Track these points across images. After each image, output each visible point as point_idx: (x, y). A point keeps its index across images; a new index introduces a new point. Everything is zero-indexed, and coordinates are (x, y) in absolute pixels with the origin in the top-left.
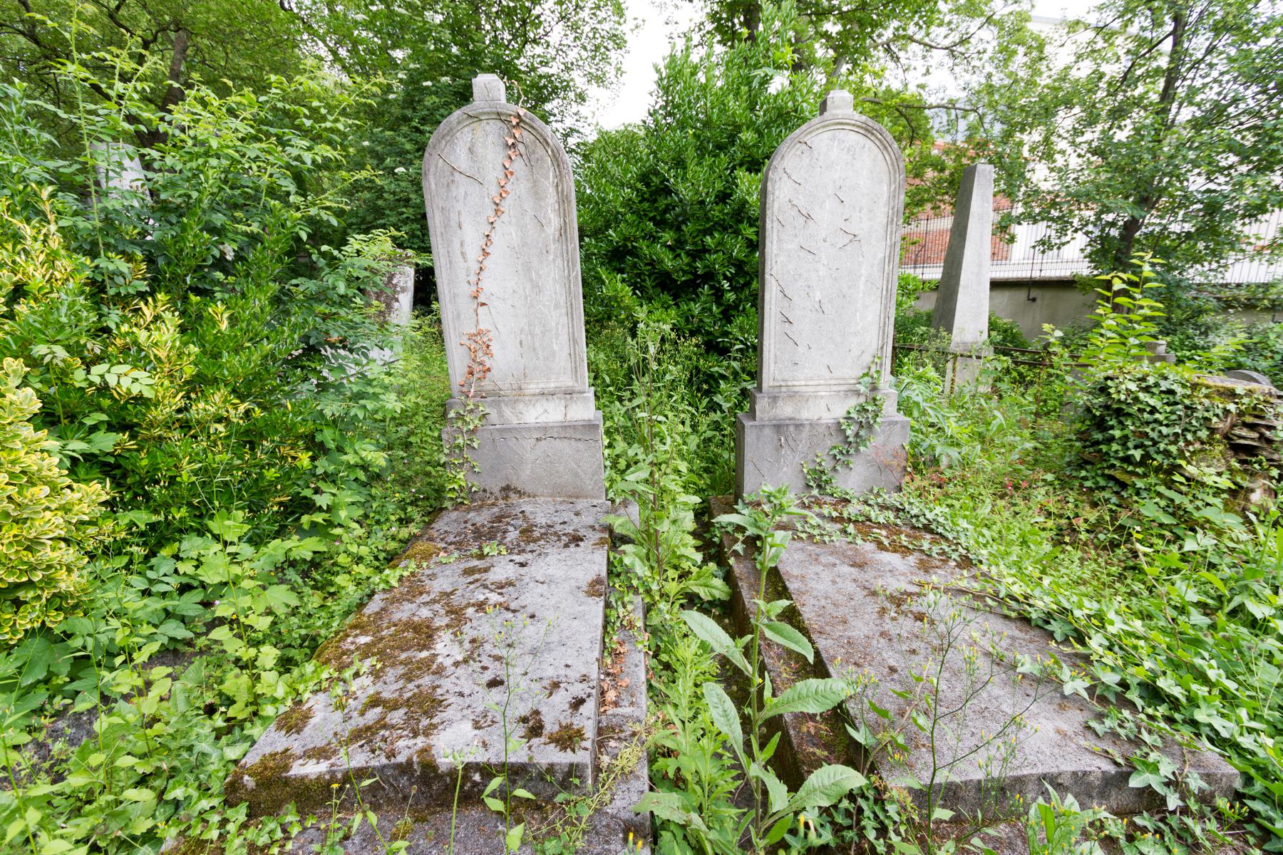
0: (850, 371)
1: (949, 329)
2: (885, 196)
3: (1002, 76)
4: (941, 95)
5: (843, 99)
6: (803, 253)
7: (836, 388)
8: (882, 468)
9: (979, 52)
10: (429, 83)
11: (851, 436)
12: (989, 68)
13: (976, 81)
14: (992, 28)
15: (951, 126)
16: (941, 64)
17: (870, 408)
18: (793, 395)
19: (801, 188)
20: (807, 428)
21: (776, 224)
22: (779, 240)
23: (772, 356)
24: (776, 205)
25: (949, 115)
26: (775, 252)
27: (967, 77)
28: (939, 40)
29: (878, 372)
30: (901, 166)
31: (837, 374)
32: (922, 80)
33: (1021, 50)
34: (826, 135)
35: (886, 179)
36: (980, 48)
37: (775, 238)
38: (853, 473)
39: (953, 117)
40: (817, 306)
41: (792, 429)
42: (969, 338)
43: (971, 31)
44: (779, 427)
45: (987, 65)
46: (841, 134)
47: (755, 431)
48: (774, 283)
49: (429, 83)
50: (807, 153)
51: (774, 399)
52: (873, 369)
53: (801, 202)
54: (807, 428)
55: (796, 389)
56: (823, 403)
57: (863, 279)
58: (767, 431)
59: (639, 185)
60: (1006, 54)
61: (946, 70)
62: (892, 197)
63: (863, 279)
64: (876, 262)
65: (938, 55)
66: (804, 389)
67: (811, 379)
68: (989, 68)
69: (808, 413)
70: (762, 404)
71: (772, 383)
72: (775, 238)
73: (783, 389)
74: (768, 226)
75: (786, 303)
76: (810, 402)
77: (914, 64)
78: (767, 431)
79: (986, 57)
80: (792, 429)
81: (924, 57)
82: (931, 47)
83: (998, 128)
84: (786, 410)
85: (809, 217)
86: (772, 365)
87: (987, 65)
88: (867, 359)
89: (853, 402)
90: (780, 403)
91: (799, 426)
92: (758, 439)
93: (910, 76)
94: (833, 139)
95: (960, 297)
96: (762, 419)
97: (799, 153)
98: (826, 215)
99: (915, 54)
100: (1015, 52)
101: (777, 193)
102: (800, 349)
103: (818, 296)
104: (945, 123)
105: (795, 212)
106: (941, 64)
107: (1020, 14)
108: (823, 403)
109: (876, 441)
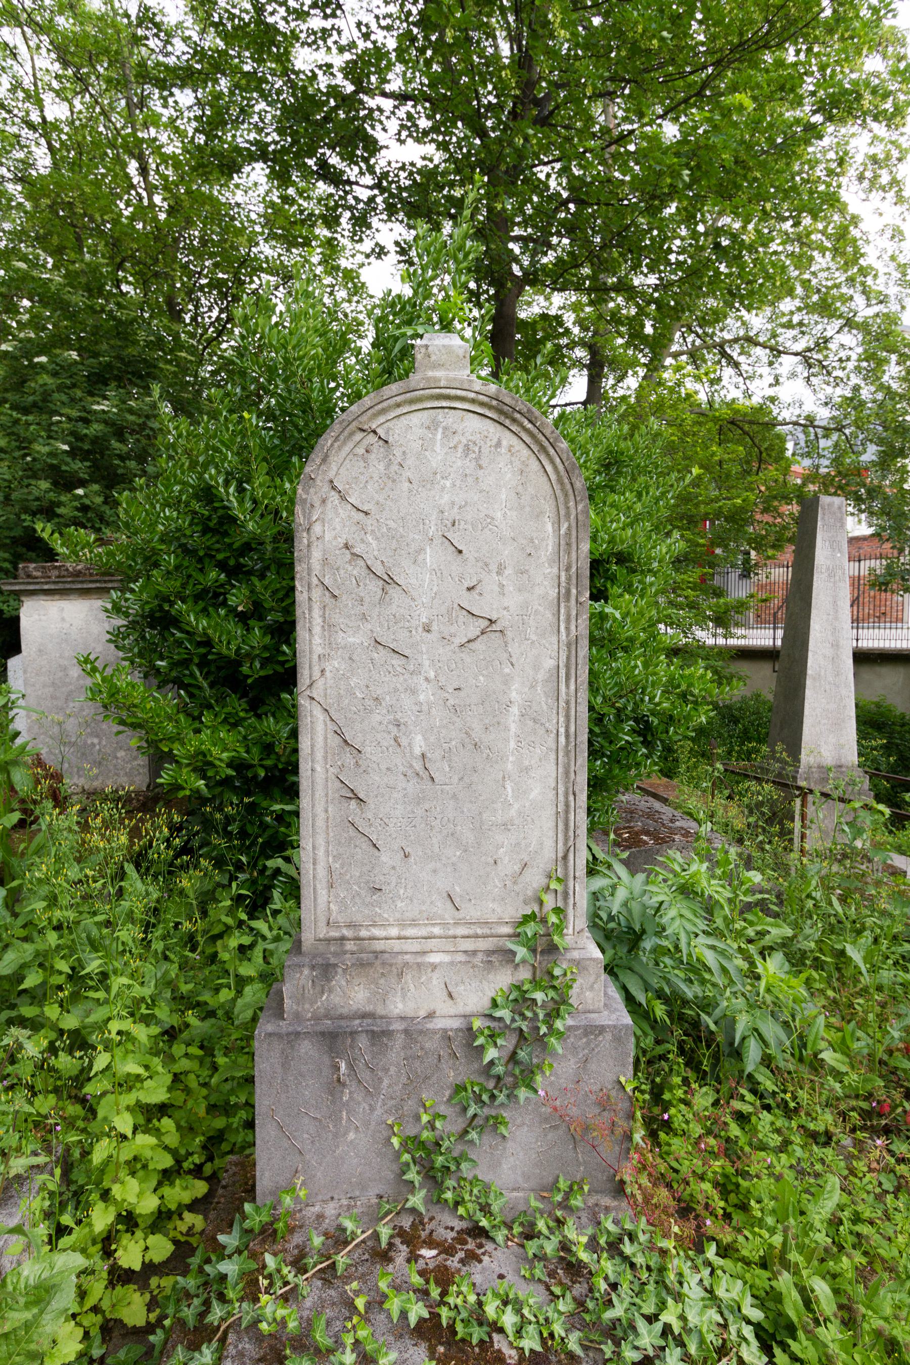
0: (500, 910)
1: (794, 747)
2: (550, 545)
3: (873, 389)
4: (797, 412)
5: (448, 349)
6: (380, 655)
7: (469, 945)
8: (578, 1134)
9: (840, 360)
10: (43, 359)
11: (506, 1054)
12: (855, 380)
13: (840, 392)
14: (854, 332)
15: (811, 450)
16: (793, 375)
17: (539, 996)
18: (371, 961)
19: (369, 521)
20: (400, 1039)
21: (316, 594)
22: (328, 626)
23: (321, 872)
24: (316, 555)
25: (806, 434)
26: (318, 650)
27: (829, 390)
28: (788, 344)
29: (558, 910)
30: (578, 485)
31: (470, 912)
32: (771, 392)
33: (894, 357)
34: (416, 419)
35: (548, 507)
36: (843, 354)
37: (317, 620)
38: (510, 1144)
39: (812, 437)
40: (418, 766)
41: (363, 1042)
42: (828, 756)
43: (828, 334)
44: (334, 1037)
45: (852, 375)
46: (450, 419)
47: (278, 1046)
48: (318, 713)
49: (43, 359)
50: (378, 449)
51: (326, 970)
52: (549, 901)
53: (371, 548)
54: (400, 1039)
55: (379, 946)
56: (436, 981)
57: (515, 710)
58: (306, 1047)
59: (196, 506)
60: (872, 364)
61: (800, 383)
62: (566, 544)
63: (515, 710)
64: (541, 676)
65: (788, 363)
66: (397, 945)
67: (414, 923)
68: (855, 380)
69: (406, 1002)
70: (296, 984)
71: (323, 932)
72: (317, 620)
73: (350, 946)
74: (301, 596)
75: (348, 759)
76: (408, 977)
77: (759, 371)
78: (306, 1047)
79: (850, 365)
80: (363, 1042)
81: (771, 364)
82: (780, 352)
83: (870, 454)
84: (353, 995)
85: (389, 581)
86: (323, 894)
87: (852, 375)
88: (535, 879)
89: (502, 980)
90: (339, 980)
91: (380, 1036)
92: (285, 1065)
93: (753, 386)
94: (433, 426)
95: (808, 693)
96: (298, 1016)
97: (361, 451)
98: (427, 578)
99: (758, 359)
100: (887, 361)
101: (317, 529)
102: (384, 858)
103: (419, 744)
104: (803, 444)
105: (358, 570)
106: (793, 375)
107: (887, 315)
108: (436, 981)
109: (558, 1073)
